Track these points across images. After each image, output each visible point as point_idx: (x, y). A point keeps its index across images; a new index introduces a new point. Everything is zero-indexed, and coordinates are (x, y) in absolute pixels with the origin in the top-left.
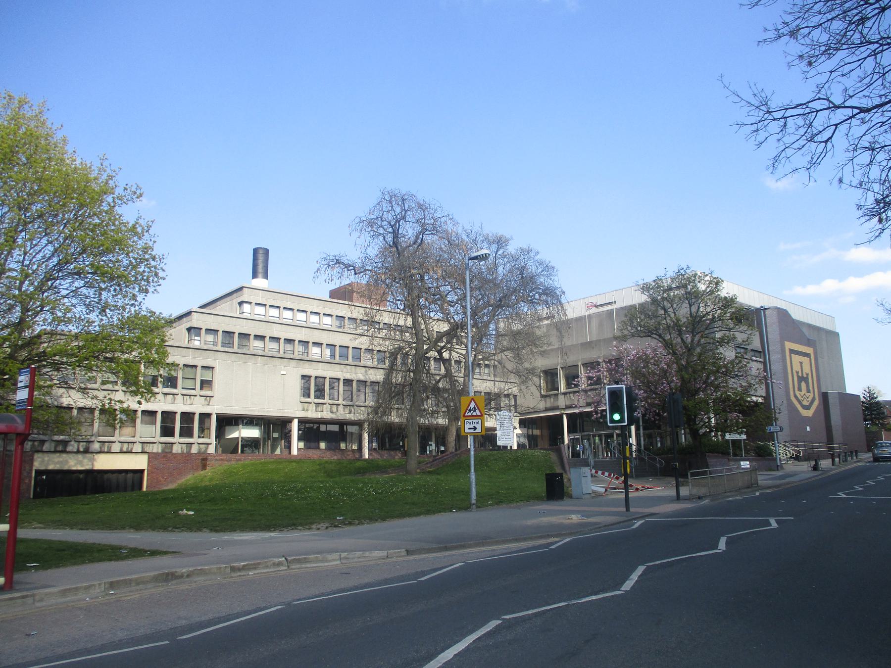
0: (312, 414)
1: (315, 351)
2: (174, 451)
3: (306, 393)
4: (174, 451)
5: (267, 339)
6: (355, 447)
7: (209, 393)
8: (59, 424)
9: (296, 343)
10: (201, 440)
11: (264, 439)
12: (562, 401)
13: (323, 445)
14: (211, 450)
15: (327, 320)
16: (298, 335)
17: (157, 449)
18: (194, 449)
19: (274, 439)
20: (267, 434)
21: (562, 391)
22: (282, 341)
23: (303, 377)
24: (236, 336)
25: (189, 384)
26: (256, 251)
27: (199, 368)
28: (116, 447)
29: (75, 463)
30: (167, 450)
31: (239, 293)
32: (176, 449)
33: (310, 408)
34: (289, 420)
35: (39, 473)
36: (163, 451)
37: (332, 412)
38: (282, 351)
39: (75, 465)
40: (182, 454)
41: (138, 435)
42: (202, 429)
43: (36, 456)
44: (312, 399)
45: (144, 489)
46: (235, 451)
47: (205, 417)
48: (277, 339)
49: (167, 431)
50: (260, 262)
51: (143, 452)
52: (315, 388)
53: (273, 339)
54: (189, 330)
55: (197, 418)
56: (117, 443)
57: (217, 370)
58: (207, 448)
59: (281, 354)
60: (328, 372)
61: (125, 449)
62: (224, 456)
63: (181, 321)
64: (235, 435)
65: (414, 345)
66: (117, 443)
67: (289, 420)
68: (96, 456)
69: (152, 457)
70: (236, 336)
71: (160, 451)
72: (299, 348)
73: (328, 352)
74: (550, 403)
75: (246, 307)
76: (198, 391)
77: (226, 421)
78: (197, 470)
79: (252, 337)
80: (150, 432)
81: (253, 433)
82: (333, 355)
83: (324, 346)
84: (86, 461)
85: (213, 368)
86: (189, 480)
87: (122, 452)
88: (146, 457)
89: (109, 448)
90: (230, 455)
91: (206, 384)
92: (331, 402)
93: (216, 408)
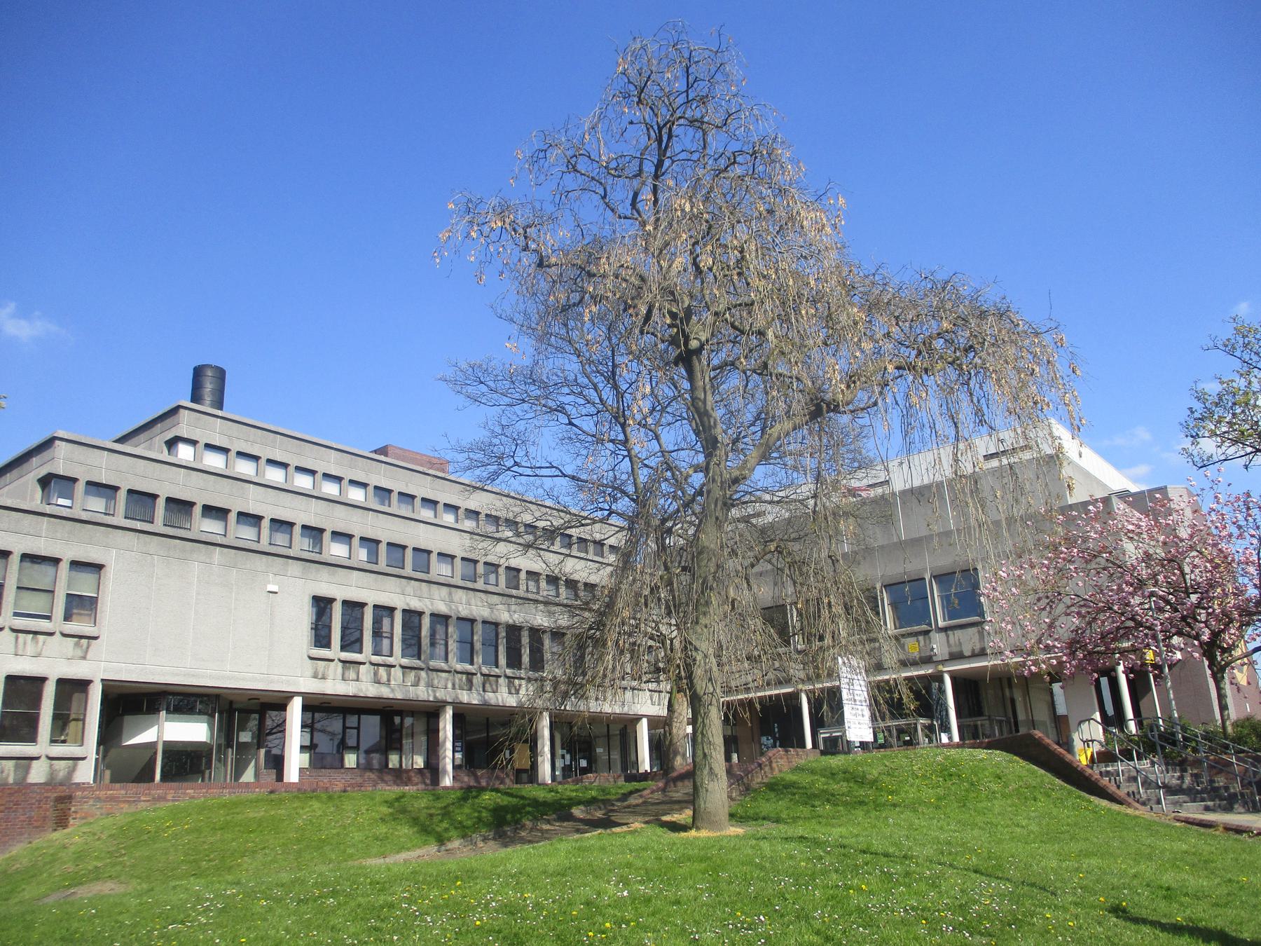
0: (336, 685)
1: (337, 550)
3: (321, 638)
5: (232, 517)
6: (419, 762)
7: (87, 629)
9: (297, 530)
10: (59, 750)
11: (219, 746)
12: (939, 645)
14: (85, 773)
15: (356, 495)
18: (38, 774)
19: (242, 747)
20: (227, 733)
21: (941, 624)
22: (265, 524)
24: (161, 503)
25: (35, 603)
26: (198, 372)
27: (64, 566)
31: (168, 422)
33: (330, 673)
37: (377, 681)
42: (62, 720)
44: (335, 651)
46: (145, 775)
47: (72, 688)
48: (254, 520)
50: (207, 384)
52: (335, 624)
53: (244, 516)
54: (45, 482)
55: (49, 692)
57: (110, 574)
58: (72, 771)
59: (264, 545)
60: (371, 592)
62: (119, 790)
63: (25, 466)
64: (148, 736)
65: (774, 455)
67: (279, 703)
70: (161, 503)
72: (301, 544)
74: (913, 647)
75: (185, 453)
76: (57, 623)
77: (128, 702)
78: (40, 828)
79: (197, 510)
83: (356, 541)
85: (98, 568)
86: (14, 859)
90: (133, 788)
91: (81, 605)
93: (103, 666)
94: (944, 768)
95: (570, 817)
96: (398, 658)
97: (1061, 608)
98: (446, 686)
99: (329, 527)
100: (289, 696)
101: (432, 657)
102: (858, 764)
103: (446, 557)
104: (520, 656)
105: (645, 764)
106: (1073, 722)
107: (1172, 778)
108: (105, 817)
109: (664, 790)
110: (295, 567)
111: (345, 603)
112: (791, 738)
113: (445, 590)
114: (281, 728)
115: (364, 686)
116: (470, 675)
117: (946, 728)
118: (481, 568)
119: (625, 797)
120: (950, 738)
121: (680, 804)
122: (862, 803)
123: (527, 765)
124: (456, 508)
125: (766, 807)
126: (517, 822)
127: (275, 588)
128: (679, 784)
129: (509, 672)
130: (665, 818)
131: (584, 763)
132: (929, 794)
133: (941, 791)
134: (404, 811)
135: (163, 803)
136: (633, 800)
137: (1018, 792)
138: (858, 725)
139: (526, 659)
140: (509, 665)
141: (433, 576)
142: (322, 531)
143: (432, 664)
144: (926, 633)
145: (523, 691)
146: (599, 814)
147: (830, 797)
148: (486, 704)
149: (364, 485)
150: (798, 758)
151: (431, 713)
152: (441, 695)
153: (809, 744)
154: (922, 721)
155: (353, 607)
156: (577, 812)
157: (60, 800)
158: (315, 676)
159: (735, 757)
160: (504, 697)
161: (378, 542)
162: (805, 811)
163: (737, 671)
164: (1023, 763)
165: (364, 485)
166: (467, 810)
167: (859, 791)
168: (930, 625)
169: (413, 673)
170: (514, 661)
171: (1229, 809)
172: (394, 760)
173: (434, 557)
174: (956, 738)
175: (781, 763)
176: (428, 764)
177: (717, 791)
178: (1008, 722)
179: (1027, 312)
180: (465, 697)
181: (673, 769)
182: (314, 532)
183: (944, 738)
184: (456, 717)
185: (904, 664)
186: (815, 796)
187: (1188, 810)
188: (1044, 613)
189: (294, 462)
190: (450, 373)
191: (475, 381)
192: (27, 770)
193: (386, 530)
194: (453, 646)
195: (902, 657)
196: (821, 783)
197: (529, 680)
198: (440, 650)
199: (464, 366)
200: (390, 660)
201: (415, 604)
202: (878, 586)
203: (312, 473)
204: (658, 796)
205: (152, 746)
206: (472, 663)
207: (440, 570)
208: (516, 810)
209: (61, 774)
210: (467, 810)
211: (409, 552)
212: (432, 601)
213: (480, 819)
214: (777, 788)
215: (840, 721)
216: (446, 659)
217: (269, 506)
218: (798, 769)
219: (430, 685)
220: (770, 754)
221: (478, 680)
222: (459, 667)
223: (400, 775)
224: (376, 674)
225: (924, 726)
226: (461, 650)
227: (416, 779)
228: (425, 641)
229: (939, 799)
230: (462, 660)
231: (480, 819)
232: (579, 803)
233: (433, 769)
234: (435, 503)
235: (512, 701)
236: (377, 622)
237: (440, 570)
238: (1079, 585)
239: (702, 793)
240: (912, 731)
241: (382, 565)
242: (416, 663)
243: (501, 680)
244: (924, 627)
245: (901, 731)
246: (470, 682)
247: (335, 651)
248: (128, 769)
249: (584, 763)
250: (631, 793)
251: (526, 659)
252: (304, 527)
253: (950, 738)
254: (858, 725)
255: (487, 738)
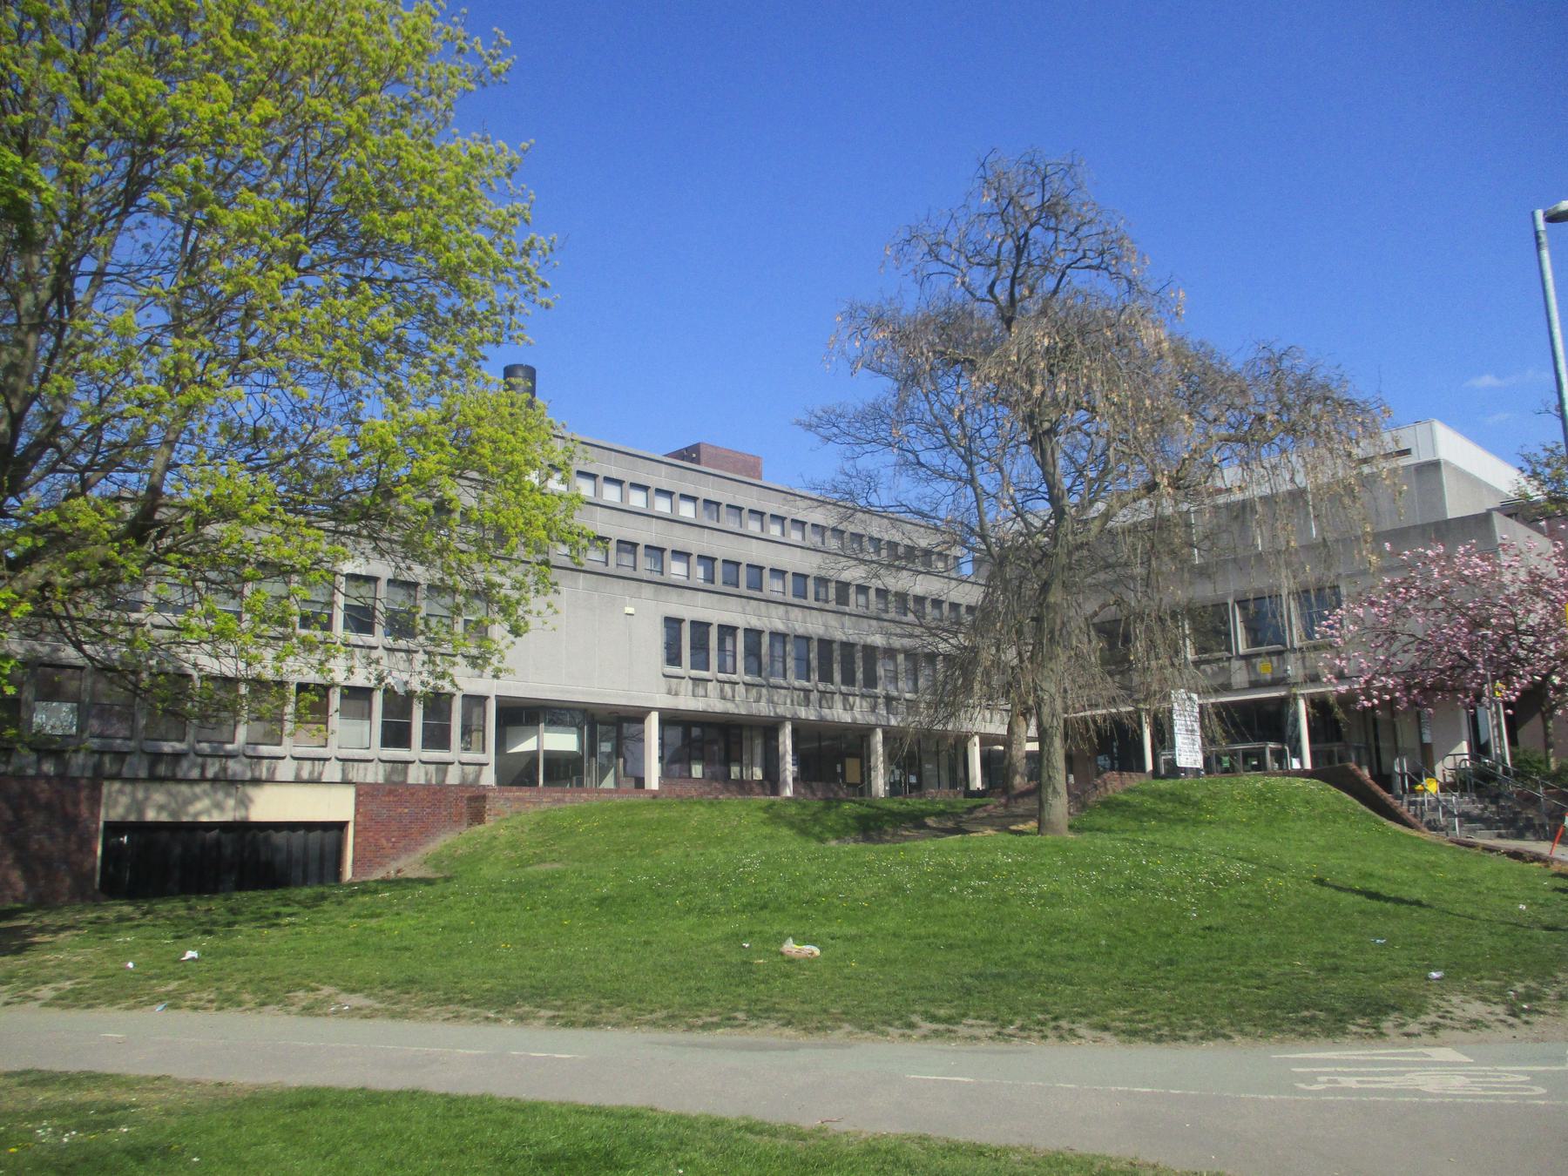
0: (688, 702)
1: (677, 569)
2: (411, 781)
3: (673, 658)
4: (411, 781)
6: (758, 774)
8: (168, 713)
9: (641, 550)
10: (468, 757)
12: (1293, 668)
13: (697, 770)
14: (489, 777)
15: (687, 511)
16: (645, 533)
17: (374, 774)
18: (453, 777)
21: (1241, 651)
23: (668, 620)
28: (286, 770)
29: (208, 808)
30: (396, 778)
32: (416, 775)
34: (637, 716)
35: (113, 828)
36: (388, 780)
37: (723, 698)
38: (612, 562)
39: (207, 811)
40: (427, 787)
41: (333, 741)
43: (108, 788)
44: (685, 669)
45: (348, 873)
49: (396, 735)
51: (345, 782)
52: (686, 643)
56: (288, 760)
59: (612, 568)
61: (305, 775)
64: (528, 745)
66: (288, 760)
67: (647, 711)
68: (253, 792)
69: (365, 794)
71: (381, 780)
72: (645, 564)
73: (700, 572)
77: (519, 714)
80: (355, 737)
81: (564, 741)
82: (710, 578)
83: (694, 559)
84: (231, 802)
87: (298, 781)
88: (349, 794)
89: (272, 771)
92: (722, 676)
94: (1261, 793)
95: (925, 826)
96: (741, 676)
97: (1396, 646)
98: (787, 702)
99: (669, 547)
100: (648, 710)
101: (772, 674)
102: (1184, 787)
103: (779, 573)
104: (854, 673)
105: (977, 782)
106: (1436, 754)
107: (1475, 809)
108: (515, 817)
109: (1006, 806)
110: (648, 590)
111: (693, 622)
112: (1129, 758)
113: (782, 608)
114: (640, 739)
115: (710, 702)
116: (807, 691)
117: (1297, 753)
118: (811, 584)
119: (971, 810)
120: (1302, 763)
121: (1025, 818)
122: (1182, 820)
123: (857, 780)
124: (783, 519)
125: (1099, 821)
126: (880, 828)
127: (630, 610)
128: (1020, 801)
129: (844, 689)
130: (1013, 828)
131: (913, 780)
132: (1242, 814)
133: (1253, 813)
134: (779, 816)
135: (542, 803)
136: (980, 814)
137: (1322, 817)
138: (1188, 752)
139: (859, 675)
140: (844, 682)
141: (766, 593)
142: (662, 550)
143: (772, 680)
144: (1280, 653)
145: (857, 709)
146: (950, 824)
147: (1158, 815)
148: (822, 719)
149: (694, 499)
150: (1134, 780)
151: (770, 729)
152: (781, 710)
153: (1149, 766)
154: (1272, 745)
155: (700, 628)
156: (930, 821)
157: (472, 799)
158: (669, 693)
159: (1072, 778)
160: (839, 714)
161: (713, 560)
162: (1133, 824)
163: (1075, 691)
164: (1334, 790)
165: (694, 499)
166: (833, 816)
167: (1179, 804)
168: (1284, 644)
169: (754, 691)
170: (849, 679)
171: (1520, 835)
172: (735, 771)
173: (766, 573)
174: (1308, 766)
175: (1116, 785)
176: (766, 774)
177: (1059, 807)
178: (1368, 749)
179: (1359, 389)
180: (803, 713)
181: (1013, 787)
182: (656, 551)
183: (1296, 764)
184: (795, 732)
185: (1255, 685)
186: (1144, 814)
187: (1481, 837)
188: (1381, 650)
189: (629, 478)
190: (805, 418)
191: (826, 425)
192: (445, 773)
193: (722, 548)
194: (791, 663)
195: (1253, 678)
196: (1149, 803)
197: (863, 696)
198: (778, 666)
199: (820, 413)
200: (734, 677)
201: (755, 623)
202: (1230, 602)
203: (645, 488)
204: (1001, 810)
205: (533, 756)
206: (808, 680)
207: (772, 586)
208: (876, 818)
209: (471, 778)
210: (833, 816)
211: (743, 569)
212: (772, 620)
213: (846, 824)
214: (1111, 806)
215: (1173, 747)
216: (785, 676)
217: (618, 528)
218: (1130, 791)
219: (770, 701)
220: (1105, 776)
221: (814, 696)
222: (797, 684)
223: (743, 786)
224: (722, 690)
225: (1273, 752)
226: (797, 666)
227: (757, 789)
228: (765, 659)
229: (1251, 818)
230: (798, 677)
231: (846, 824)
232: (930, 814)
233: (772, 779)
234: (762, 514)
235: (847, 718)
236: (721, 642)
237: (772, 586)
238: (1418, 623)
239: (1047, 807)
240: (1260, 755)
241: (719, 585)
242: (758, 680)
243: (837, 697)
244: (1279, 647)
245: (1247, 755)
246: (807, 699)
247: (685, 669)
248: (519, 774)
249: (913, 780)
250: (975, 807)
251: (859, 675)
252: (647, 547)
253: (1302, 763)
254: (1188, 752)
255: (830, 755)
